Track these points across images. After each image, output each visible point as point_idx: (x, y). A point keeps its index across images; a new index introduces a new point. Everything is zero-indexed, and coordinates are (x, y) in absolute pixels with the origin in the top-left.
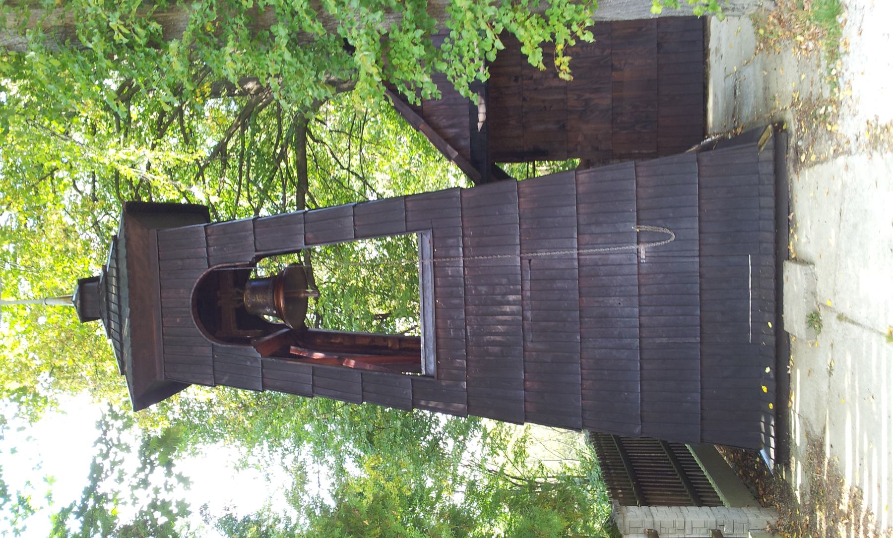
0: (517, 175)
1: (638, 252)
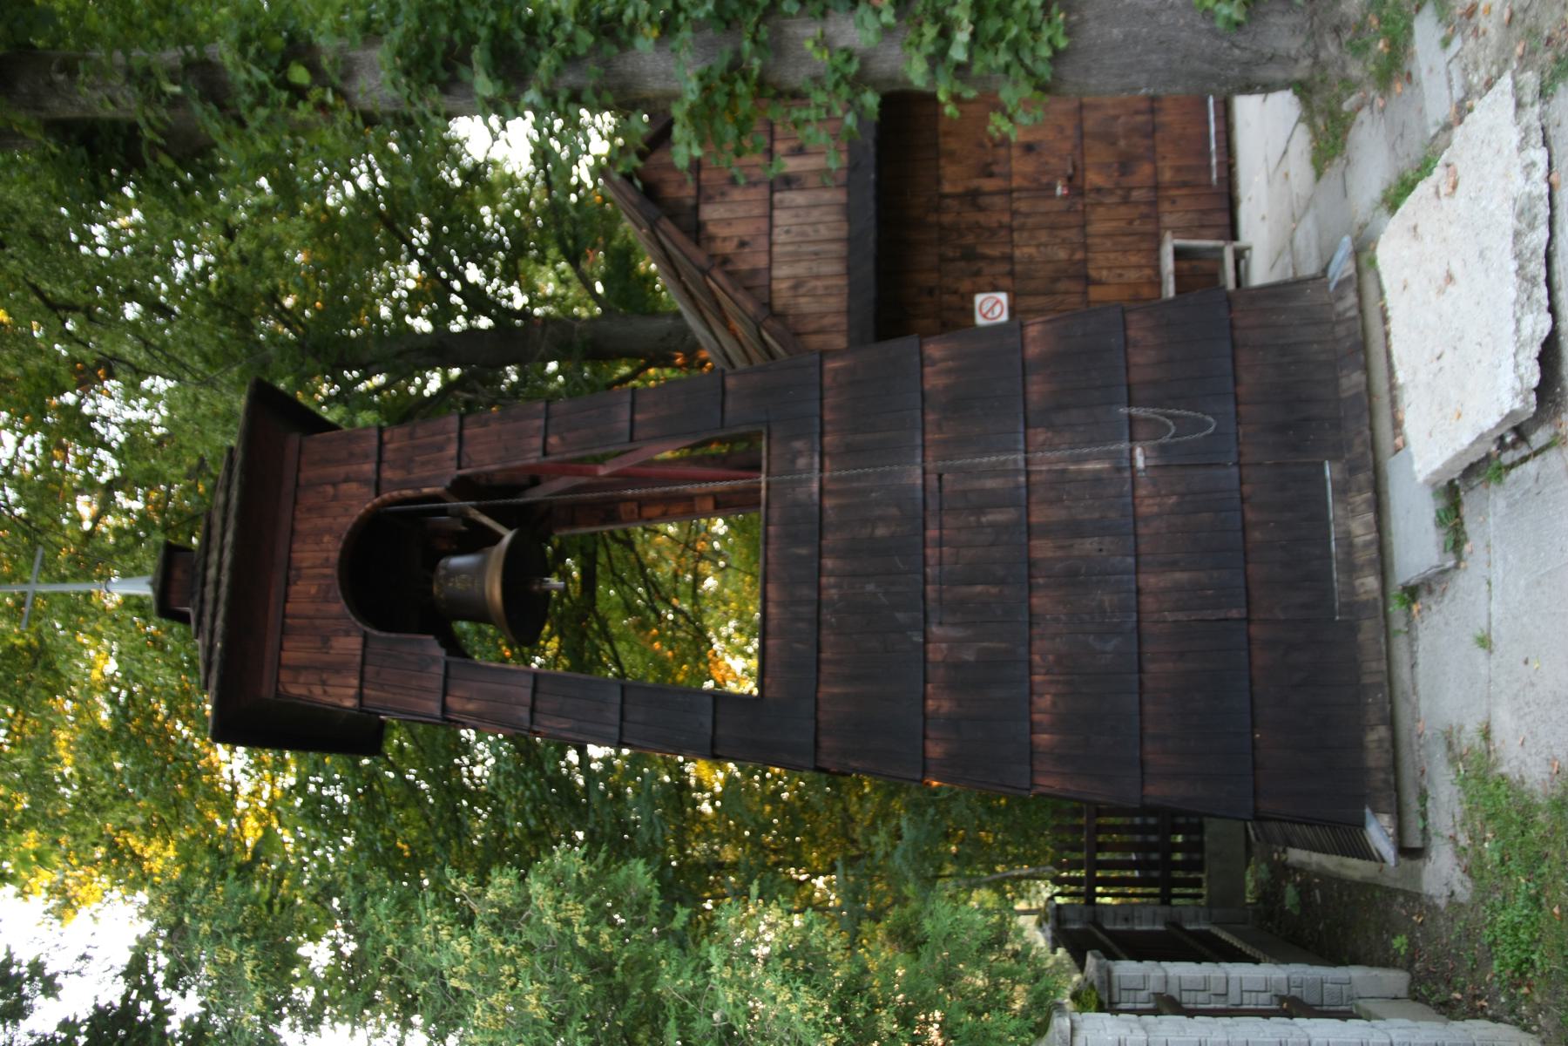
1: (1132, 459)
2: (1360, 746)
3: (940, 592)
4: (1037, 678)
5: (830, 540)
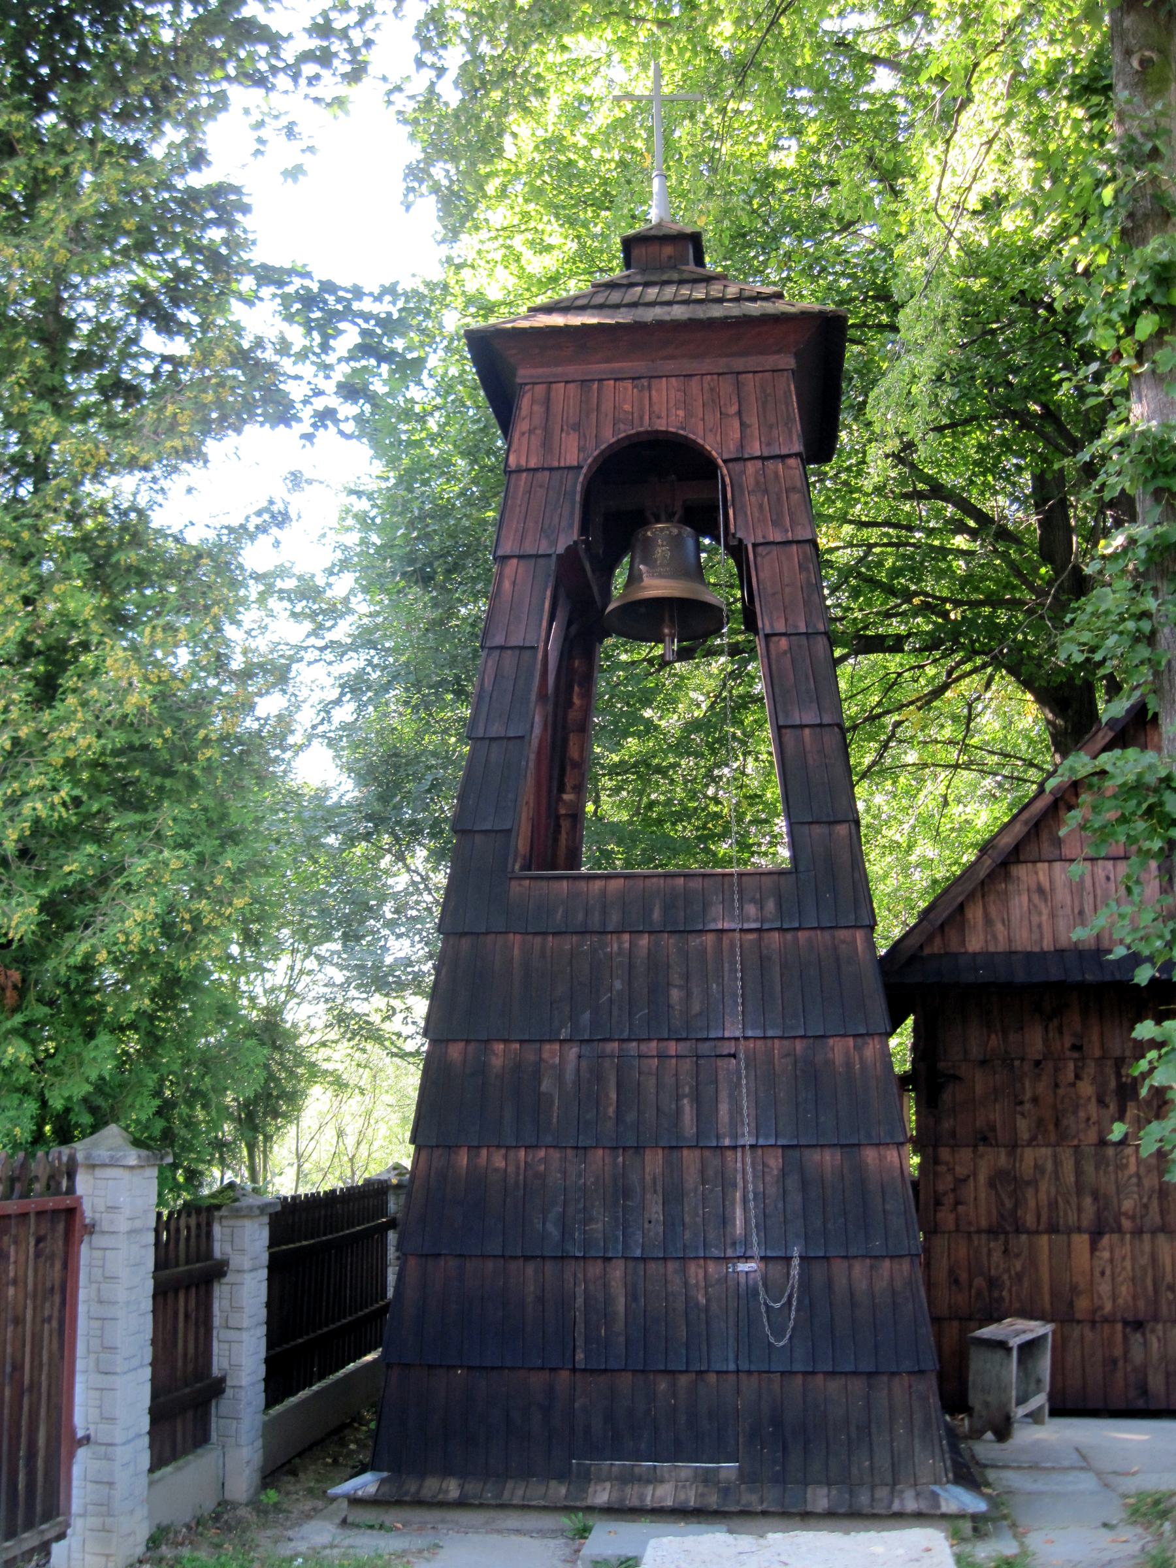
0: (893, 1042)
1: (747, 1258)
2: (447, 1471)
3: (612, 1056)
4: (522, 1153)
5: (670, 942)
